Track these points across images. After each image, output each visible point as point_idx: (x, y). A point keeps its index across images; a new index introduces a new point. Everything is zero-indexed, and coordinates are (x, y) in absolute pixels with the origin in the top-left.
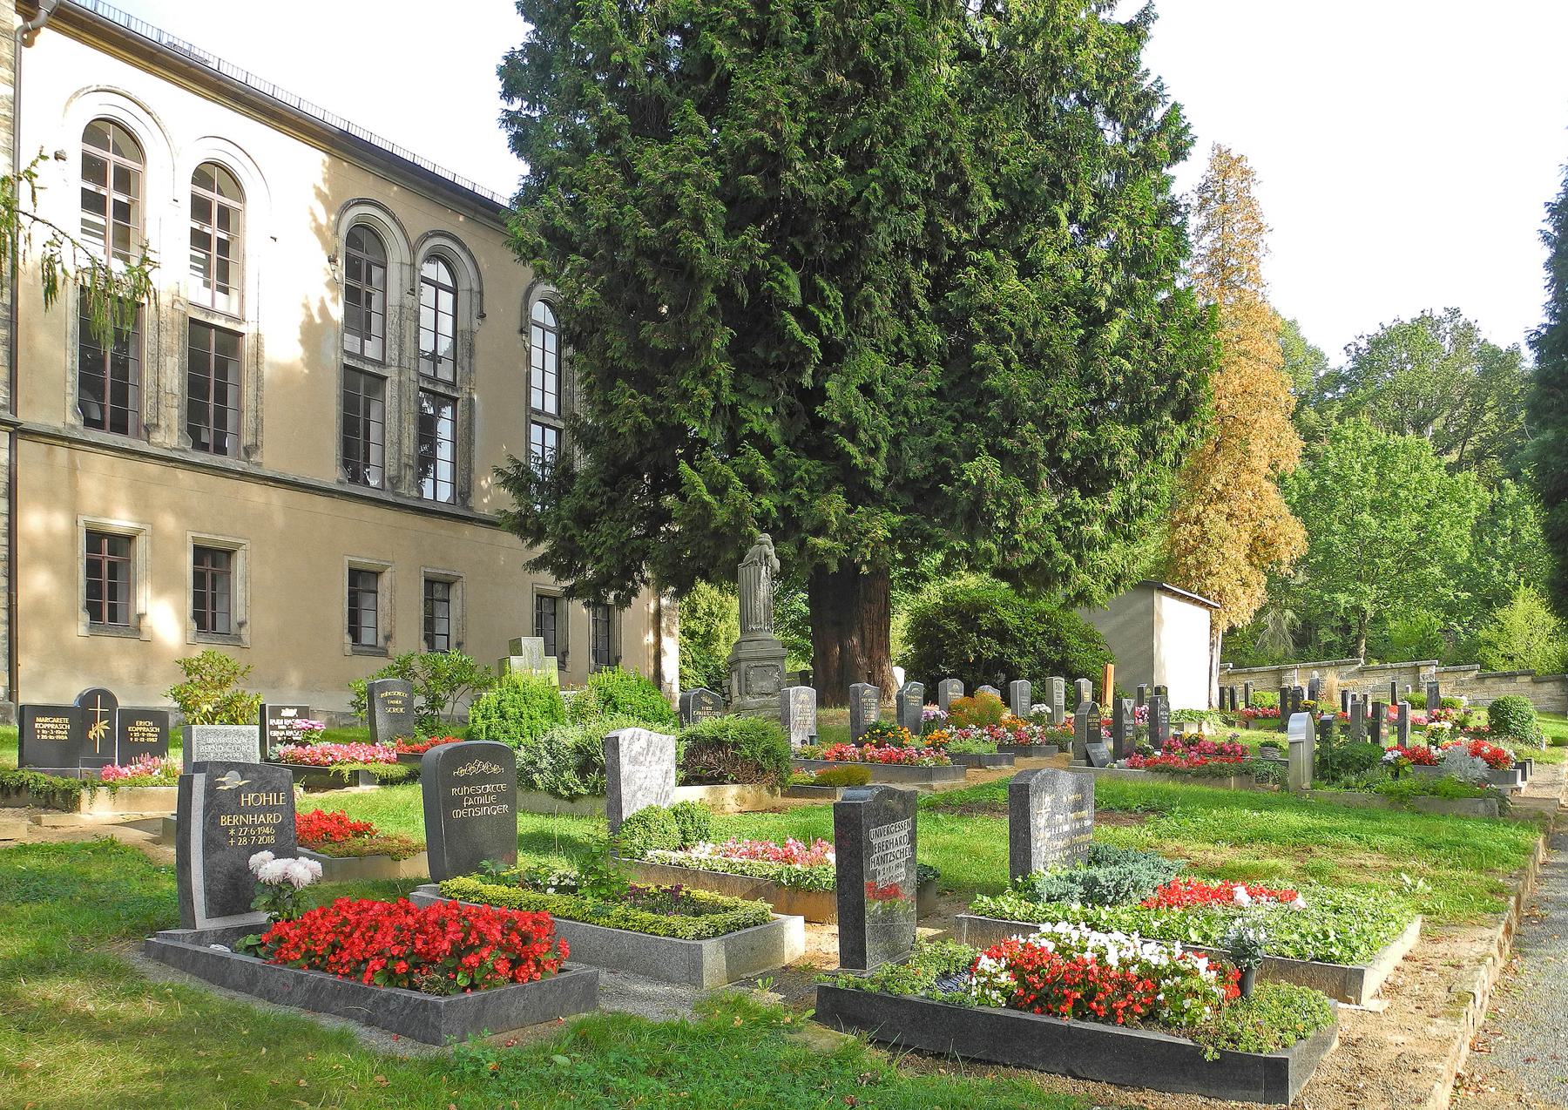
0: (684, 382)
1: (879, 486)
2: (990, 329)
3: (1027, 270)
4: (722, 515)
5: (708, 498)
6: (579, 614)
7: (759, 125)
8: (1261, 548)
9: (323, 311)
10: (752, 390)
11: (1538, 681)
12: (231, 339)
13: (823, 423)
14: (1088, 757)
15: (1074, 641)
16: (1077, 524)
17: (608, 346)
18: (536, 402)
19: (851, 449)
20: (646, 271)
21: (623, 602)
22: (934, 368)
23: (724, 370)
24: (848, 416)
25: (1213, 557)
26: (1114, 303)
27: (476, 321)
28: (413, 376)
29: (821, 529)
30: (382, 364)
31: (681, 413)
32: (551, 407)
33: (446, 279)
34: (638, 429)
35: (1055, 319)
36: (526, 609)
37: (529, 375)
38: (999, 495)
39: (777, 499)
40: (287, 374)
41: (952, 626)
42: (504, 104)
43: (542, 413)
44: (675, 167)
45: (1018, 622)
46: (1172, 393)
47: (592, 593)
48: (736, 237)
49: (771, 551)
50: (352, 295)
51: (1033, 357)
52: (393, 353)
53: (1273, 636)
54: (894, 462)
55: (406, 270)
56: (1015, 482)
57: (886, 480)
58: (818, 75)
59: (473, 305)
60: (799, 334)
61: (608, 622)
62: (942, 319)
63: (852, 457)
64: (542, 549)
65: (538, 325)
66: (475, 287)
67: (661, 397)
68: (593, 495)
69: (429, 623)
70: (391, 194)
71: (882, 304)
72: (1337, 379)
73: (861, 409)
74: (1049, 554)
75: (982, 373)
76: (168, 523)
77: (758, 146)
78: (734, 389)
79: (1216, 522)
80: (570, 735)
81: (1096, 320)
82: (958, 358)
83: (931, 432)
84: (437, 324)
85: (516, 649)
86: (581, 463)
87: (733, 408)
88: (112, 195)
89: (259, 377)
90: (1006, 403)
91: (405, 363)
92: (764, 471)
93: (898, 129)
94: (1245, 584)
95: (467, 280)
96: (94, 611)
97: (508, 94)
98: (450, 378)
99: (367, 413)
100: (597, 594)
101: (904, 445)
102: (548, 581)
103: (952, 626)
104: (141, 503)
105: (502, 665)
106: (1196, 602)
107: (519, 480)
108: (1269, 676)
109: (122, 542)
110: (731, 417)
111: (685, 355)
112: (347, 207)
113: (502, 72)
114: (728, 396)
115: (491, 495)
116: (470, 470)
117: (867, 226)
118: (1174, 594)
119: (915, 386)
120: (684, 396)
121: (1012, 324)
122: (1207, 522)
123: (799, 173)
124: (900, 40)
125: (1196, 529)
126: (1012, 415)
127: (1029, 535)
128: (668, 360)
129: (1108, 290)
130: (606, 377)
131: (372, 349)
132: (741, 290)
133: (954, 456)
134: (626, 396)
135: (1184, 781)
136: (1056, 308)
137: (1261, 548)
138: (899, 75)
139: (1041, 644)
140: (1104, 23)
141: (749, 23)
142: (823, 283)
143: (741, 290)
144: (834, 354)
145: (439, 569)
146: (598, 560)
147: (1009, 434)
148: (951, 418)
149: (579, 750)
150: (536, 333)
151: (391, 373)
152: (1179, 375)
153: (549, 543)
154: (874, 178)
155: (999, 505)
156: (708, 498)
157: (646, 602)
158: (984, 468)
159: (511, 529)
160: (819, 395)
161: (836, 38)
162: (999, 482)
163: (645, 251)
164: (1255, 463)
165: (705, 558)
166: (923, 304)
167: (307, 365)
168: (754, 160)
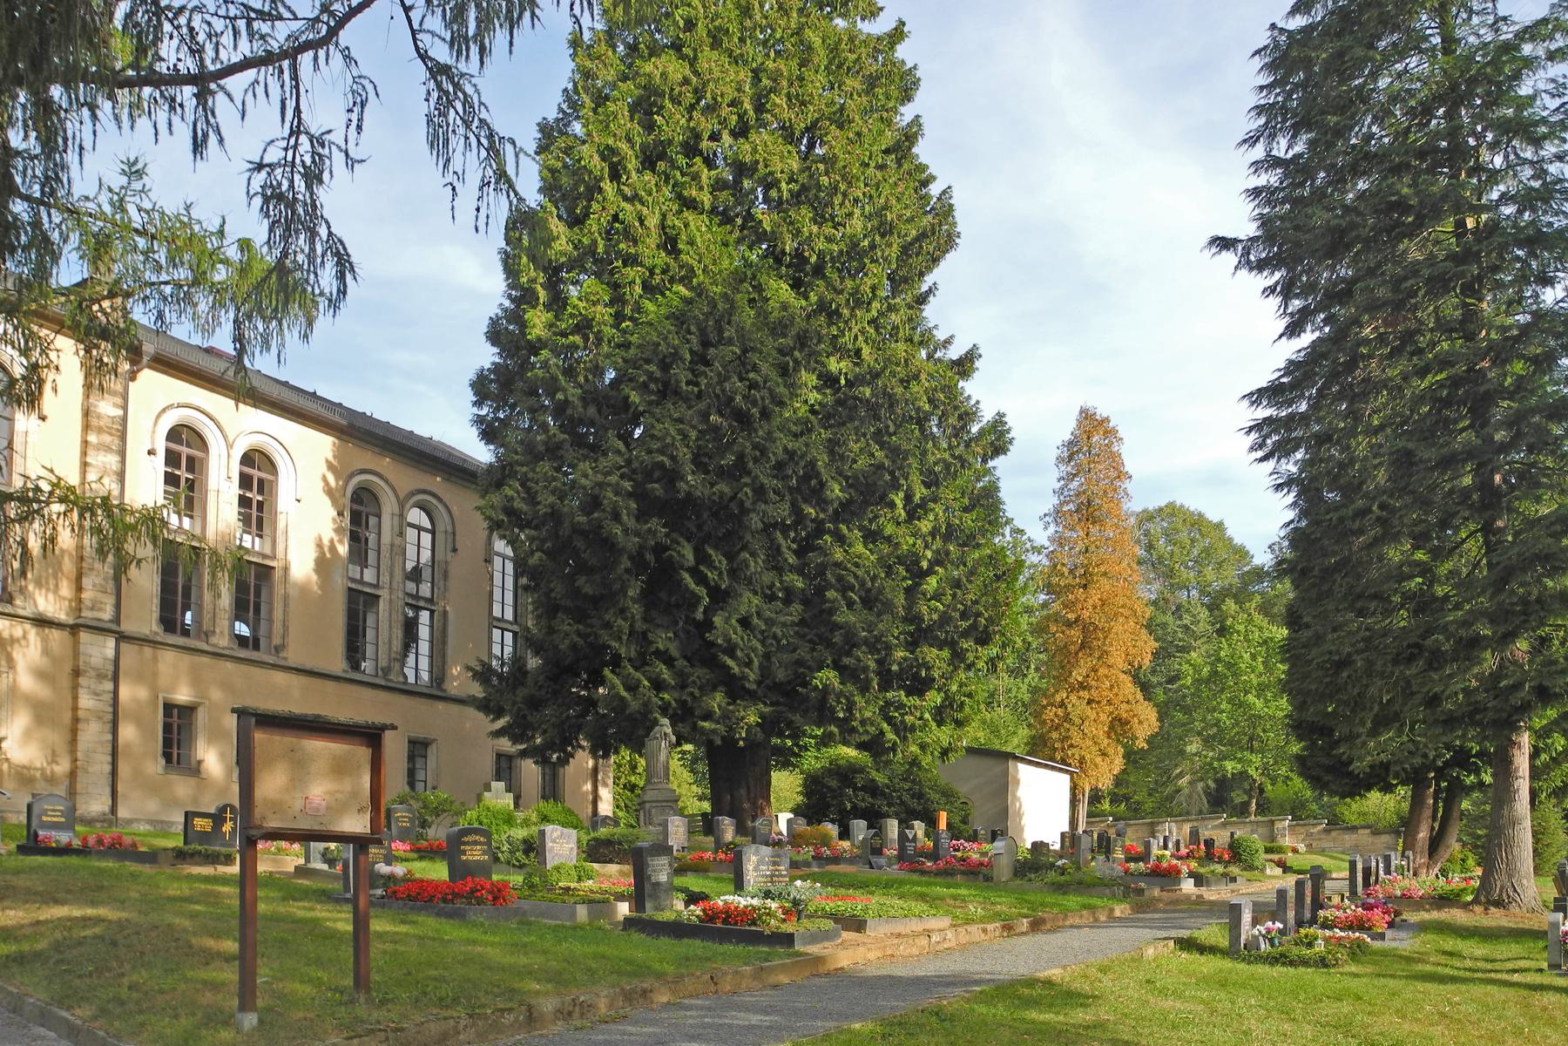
0: (607, 617)
2: (840, 579)
3: (871, 537)
4: (634, 706)
5: (624, 694)
6: (530, 770)
7: (661, 452)
8: (1119, 727)
9: (332, 548)
10: (659, 621)
11: (1376, 832)
12: (264, 572)
13: (713, 644)
15: (934, 796)
16: (902, 715)
17: (552, 590)
18: (497, 612)
19: (730, 662)
20: (579, 543)
21: (564, 762)
22: (796, 607)
23: (636, 610)
24: (729, 640)
25: (1074, 732)
26: (932, 564)
27: (450, 554)
28: (401, 595)
29: (708, 716)
30: (377, 586)
31: (605, 637)
32: (509, 615)
33: (426, 523)
34: (574, 647)
35: (888, 574)
36: (488, 763)
37: (491, 593)
38: (841, 694)
39: (676, 695)
40: (304, 589)
41: (834, 783)
42: (475, 410)
43: (502, 620)
44: (600, 477)
46: (974, 626)
47: (540, 755)
48: (647, 522)
49: (669, 730)
50: (355, 538)
51: (871, 600)
52: (385, 578)
53: (1190, 796)
54: (765, 671)
55: (396, 519)
56: (850, 687)
57: (759, 683)
58: (705, 416)
59: (446, 538)
60: (693, 586)
61: (554, 776)
64: (501, 723)
65: (499, 554)
66: (449, 529)
67: (592, 626)
68: (540, 688)
69: (411, 773)
70: (385, 464)
71: (755, 565)
72: (1259, 574)
73: (737, 635)
74: (882, 733)
75: (831, 612)
76: (216, 694)
77: (661, 465)
78: (645, 619)
79: (1077, 704)
80: (520, 833)
81: (920, 575)
82: (814, 601)
83: (794, 651)
84: (420, 549)
85: (488, 788)
86: (533, 663)
87: (644, 634)
88: (183, 474)
89: (286, 597)
90: (847, 633)
91: (395, 585)
92: (666, 675)
93: (763, 451)
94: (1104, 754)
95: (443, 523)
96: (168, 756)
97: (478, 404)
98: (428, 595)
99: (365, 621)
100: (543, 756)
102: (505, 744)
103: (834, 783)
104: (196, 681)
105: (479, 798)
106: (1061, 770)
107: (483, 674)
108: (1144, 828)
109: (188, 711)
110: (643, 639)
111: (607, 598)
112: (352, 476)
113: (473, 385)
114: (640, 626)
115: (459, 679)
116: (444, 663)
117: (744, 511)
119: (783, 619)
120: (608, 625)
121: (856, 577)
123: (692, 480)
124: (765, 393)
125: (1060, 712)
126: (851, 643)
127: (863, 722)
128: (596, 601)
130: (549, 610)
131: (369, 575)
132: (649, 557)
133: (809, 668)
134: (565, 625)
136: (890, 567)
137: (1119, 727)
138: (765, 414)
139: (906, 797)
140: (939, 360)
141: (656, 380)
142: (711, 551)
143: (649, 557)
144: (720, 597)
145: (420, 734)
146: (545, 732)
147: (849, 654)
148: (810, 641)
149: (525, 841)
150: (498, 561)
151: (384, 593)
152: (979, 614)
153: (507, 719)
154: (746, 485)
155: (839, 702)
156: (624, 694)
157: (584, 760)
158: (828, 677)
159: (479, 708)
160: (708, 625)
161: (717, 396)
163: (577, 530)
164: (1111, 661)
165: (622, 732)
166: (792, 559)
167: (321, 588)
168: (657, 474)
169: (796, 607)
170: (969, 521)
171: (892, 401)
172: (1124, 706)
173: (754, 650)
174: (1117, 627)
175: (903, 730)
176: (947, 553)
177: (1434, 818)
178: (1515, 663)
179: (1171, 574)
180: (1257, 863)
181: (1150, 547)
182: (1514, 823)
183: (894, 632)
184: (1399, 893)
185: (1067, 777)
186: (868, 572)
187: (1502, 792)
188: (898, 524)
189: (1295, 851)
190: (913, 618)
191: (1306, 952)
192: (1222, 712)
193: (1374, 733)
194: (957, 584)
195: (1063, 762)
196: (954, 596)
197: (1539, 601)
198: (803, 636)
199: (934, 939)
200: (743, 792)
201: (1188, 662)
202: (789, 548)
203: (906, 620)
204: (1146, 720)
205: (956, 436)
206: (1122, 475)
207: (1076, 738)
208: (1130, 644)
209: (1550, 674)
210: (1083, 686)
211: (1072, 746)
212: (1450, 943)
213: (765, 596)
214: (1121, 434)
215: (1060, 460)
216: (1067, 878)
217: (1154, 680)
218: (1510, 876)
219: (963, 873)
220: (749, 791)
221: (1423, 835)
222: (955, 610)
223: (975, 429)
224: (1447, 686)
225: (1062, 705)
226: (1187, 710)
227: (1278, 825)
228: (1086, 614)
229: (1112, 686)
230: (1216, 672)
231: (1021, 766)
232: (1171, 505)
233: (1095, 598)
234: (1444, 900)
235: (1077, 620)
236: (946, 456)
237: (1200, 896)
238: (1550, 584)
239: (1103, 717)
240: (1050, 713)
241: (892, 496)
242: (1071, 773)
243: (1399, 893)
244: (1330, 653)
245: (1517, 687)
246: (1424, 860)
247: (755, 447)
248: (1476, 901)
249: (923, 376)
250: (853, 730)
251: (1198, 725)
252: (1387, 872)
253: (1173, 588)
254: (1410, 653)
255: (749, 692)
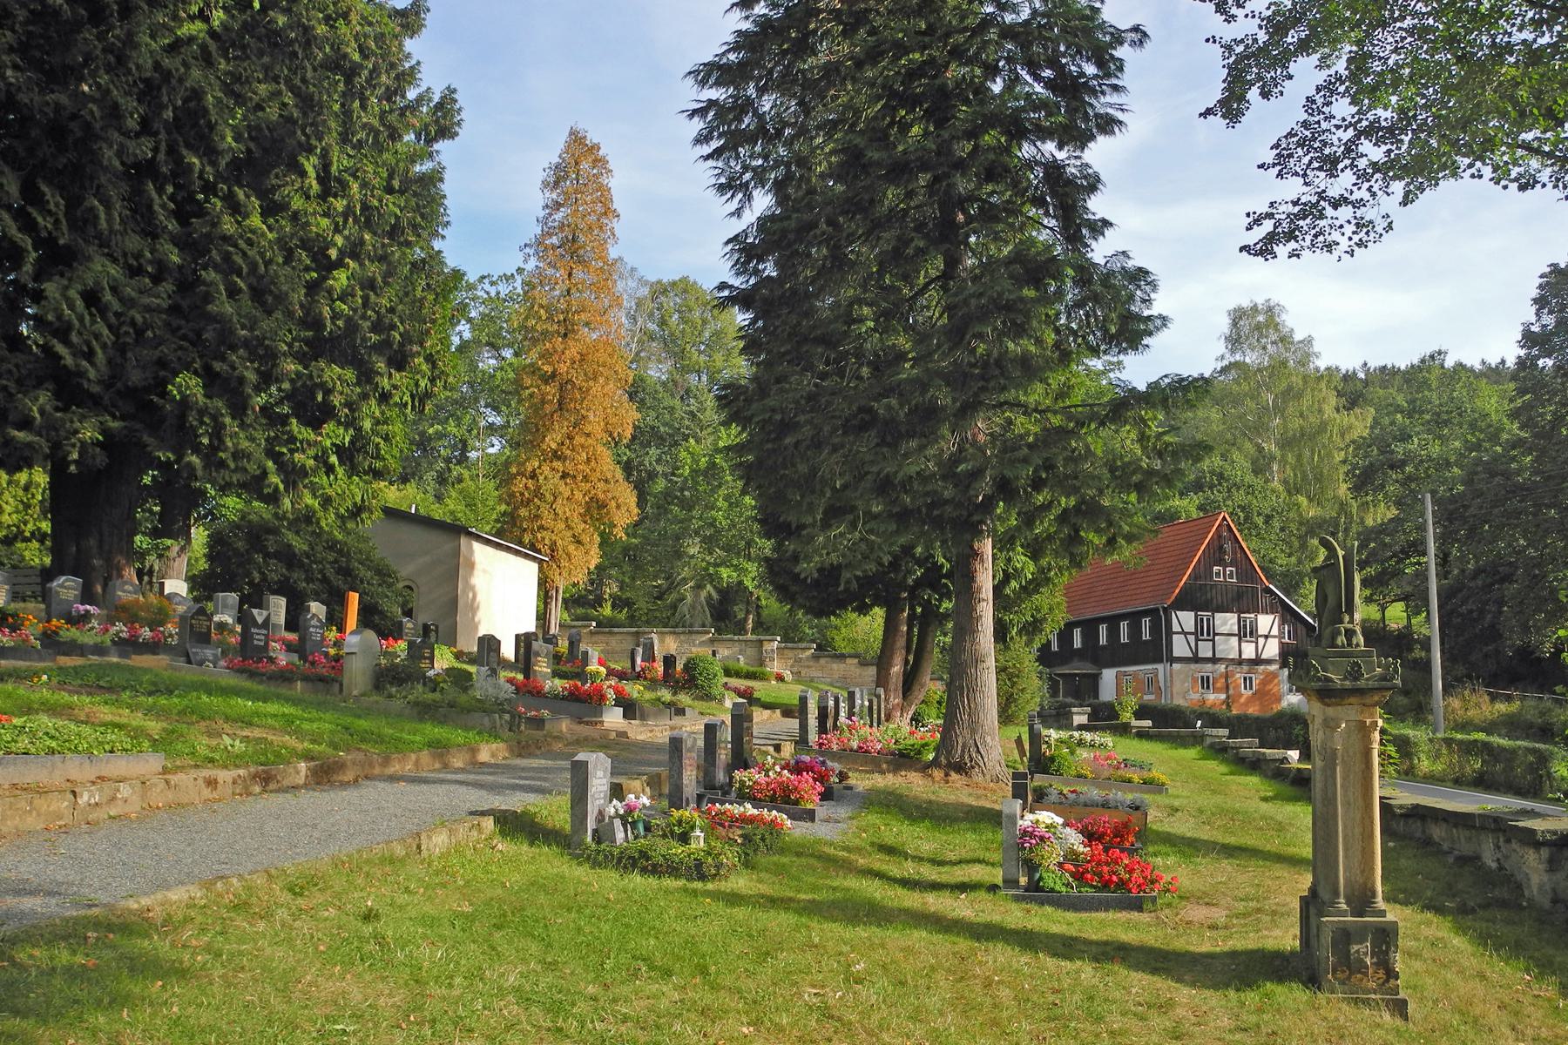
1: (96, 389)
2: (227, 257)
3: (272, 209)
14: (188, 656)
16: (292, 451)
29: (26, 424)
38: (202, 412)
45: (305, 548)
51: (264, 295)
53: (693, 607)
62: (182, 243)
63: (61, 358)
71: (109, 215)
74: (265, 474)
79: (550, 479)
81: (331, 266)
82: (187, 284)
94: (579, 542)
101: (130, 355)
103: (240, 545)
106: (526, 556)
108: (629, 638)
118: (487, 542)
119: (146, 300)
122: (541, 478)
127: (238, 455)
129: (339, 240)
135: (261, 682)
137: (596, 509)
139: (330, 572)
142: (44, 188)
152: (393, 327)
155: (202, 423)
158: (188, 385)
162: (201, 399)
169: (167, 287)
170: (392, 205)
171: (308, 38)
172: (601, 485)
173: (97, 336)
174: (596, 389)
175: (294, 476)
176: (362, 242)
177: (908, 652)
178: (974, 443)
179: (681, 355)
180: (715, 692)
181: (663, 323)
182: (977, 660)
183: (285, 337)
184: (855, 744)
185: (536, 566)
186: (262, 255)
187: (966, 625)
188: (308, 197)
189: (780, 678)
190: (312, 321)
191: (678, 850)
192: (720, 509)
193: (826, 525)
194: (370, 285)
195: (533, 547)
196: (366, 299)
197: (998, 363)
198: (174, 331)
199: (84, 799)
200: (92, 542)
201: (687, 449)
202: (163, 206)
203: (304, 323)
204: (625, 507)
205: (389, 100)
206: (609, 212)
207: (547, 520)
208: (609, 412)
209: (1012, 462)
210: (557, 456)
211: (541, 528)
212: (897, 831)
213: (130, 267)
214: (611, 166)
215: (545, 184)
216: (437, 696)
217: (659, 469)
218: (973, 732)
219: (306, 679)
220: (101, 541)
221: (897, 669)
222: (364, 317)
223: (412, 94)
224: (900, 466)
225: (533, 476)
226: (688, 506)
227: (767, 646)
228: (563, 368)
229: (589, 460)
230: (714, 464)
231: (476, 546)
232: (684, 280)
233: (573, 351)
234: (904, 759)
235: (554, 375)
236: (376, 122)
237: (623, 734)
238: (1011, 345)
239: (578, 495)
240: (520, 484)
241: (302, 160)
242: (540, 562)
243: (855, 744)
244: (773, 410)
245: (976, 474)
246: (896, 700)
247: (108, 50)
248: (935, 763)
249: (354, 18)
250: (222, 464)
251: (695, 524)
252: (850, 715)
253: (685, 370)
254: (863, 421)
255: (92, 396)
